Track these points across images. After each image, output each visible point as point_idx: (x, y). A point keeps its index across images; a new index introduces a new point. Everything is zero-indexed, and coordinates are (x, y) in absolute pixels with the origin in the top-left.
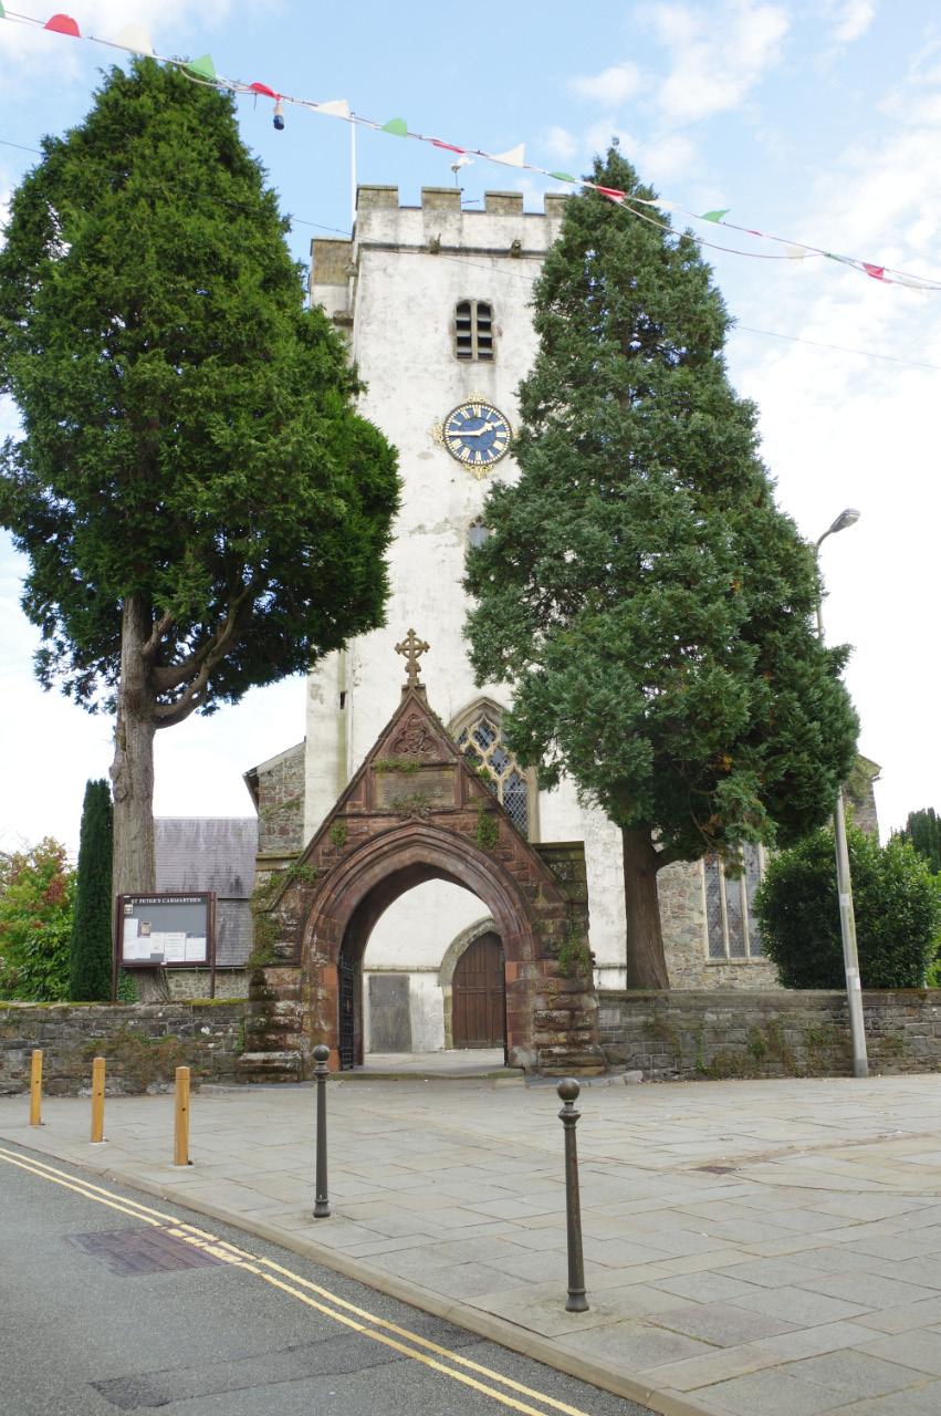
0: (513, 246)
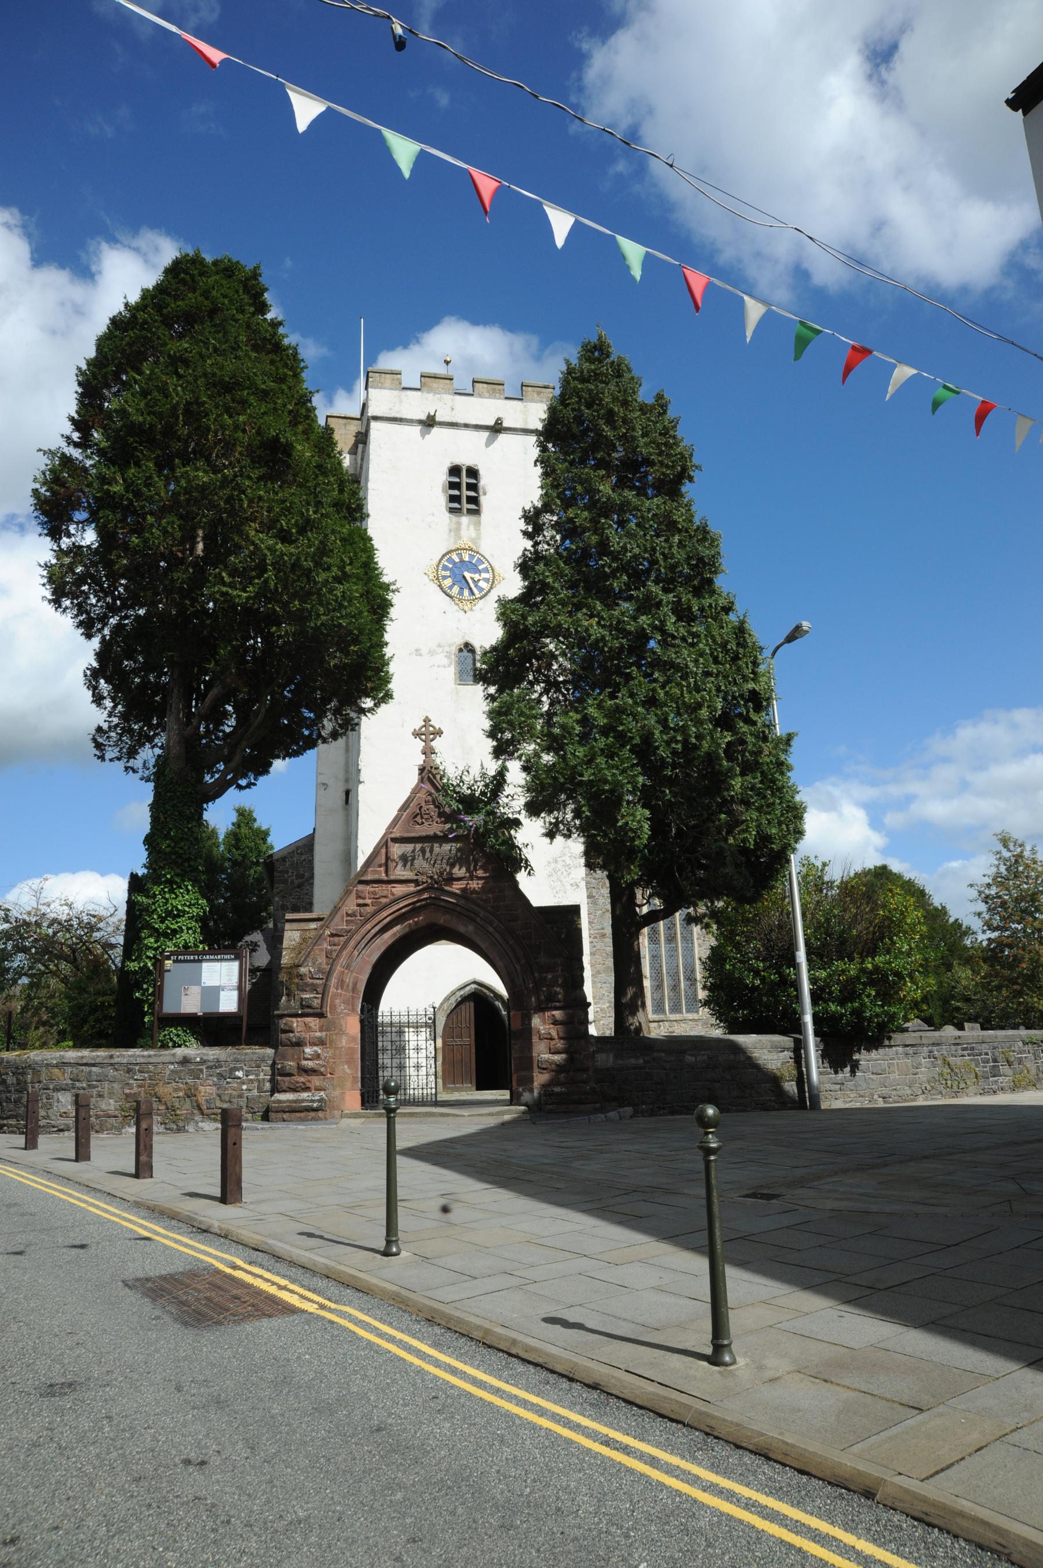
0: (496, 423)
